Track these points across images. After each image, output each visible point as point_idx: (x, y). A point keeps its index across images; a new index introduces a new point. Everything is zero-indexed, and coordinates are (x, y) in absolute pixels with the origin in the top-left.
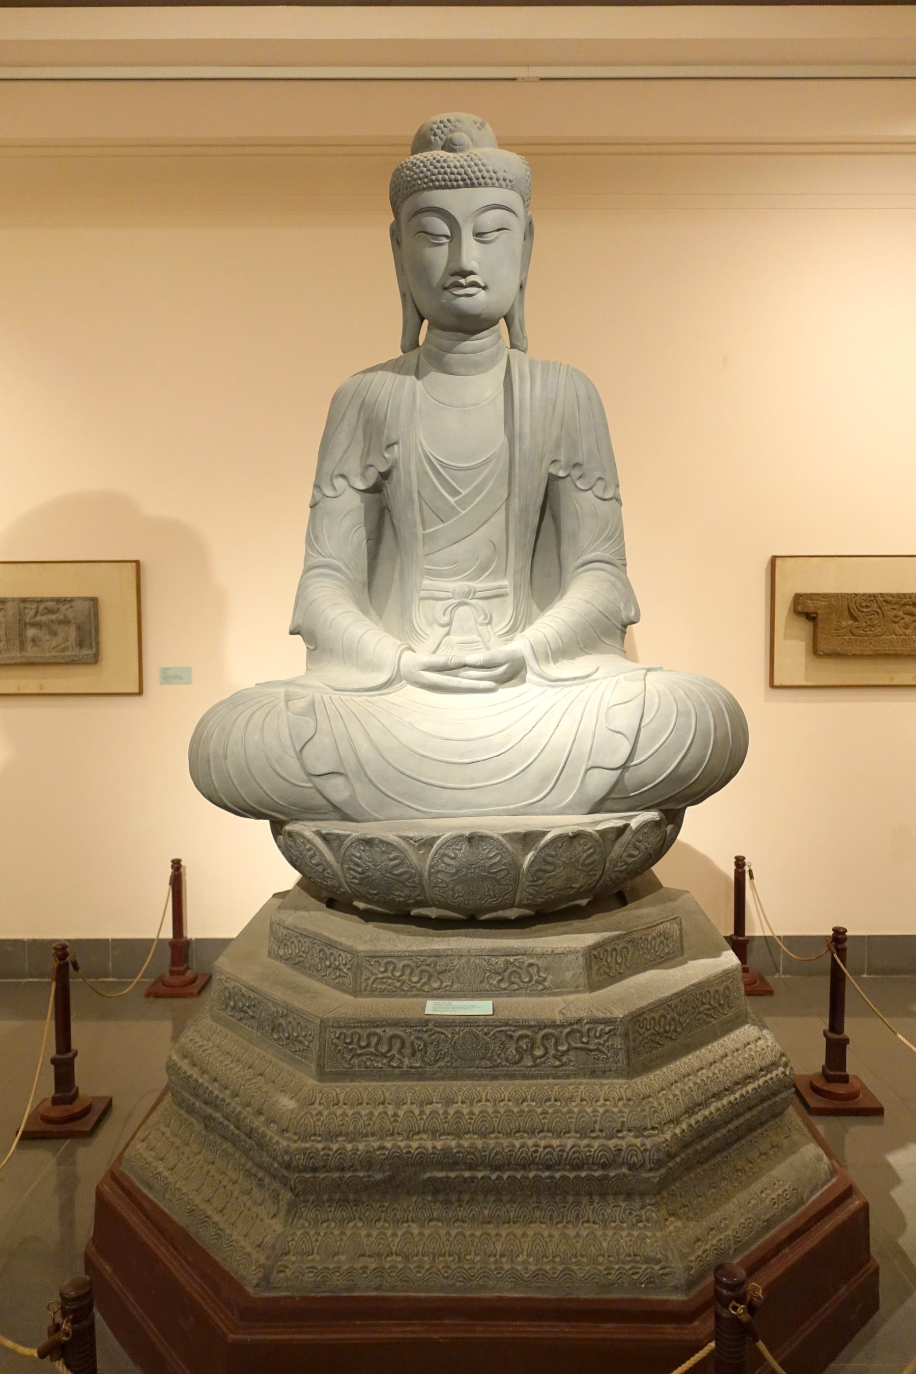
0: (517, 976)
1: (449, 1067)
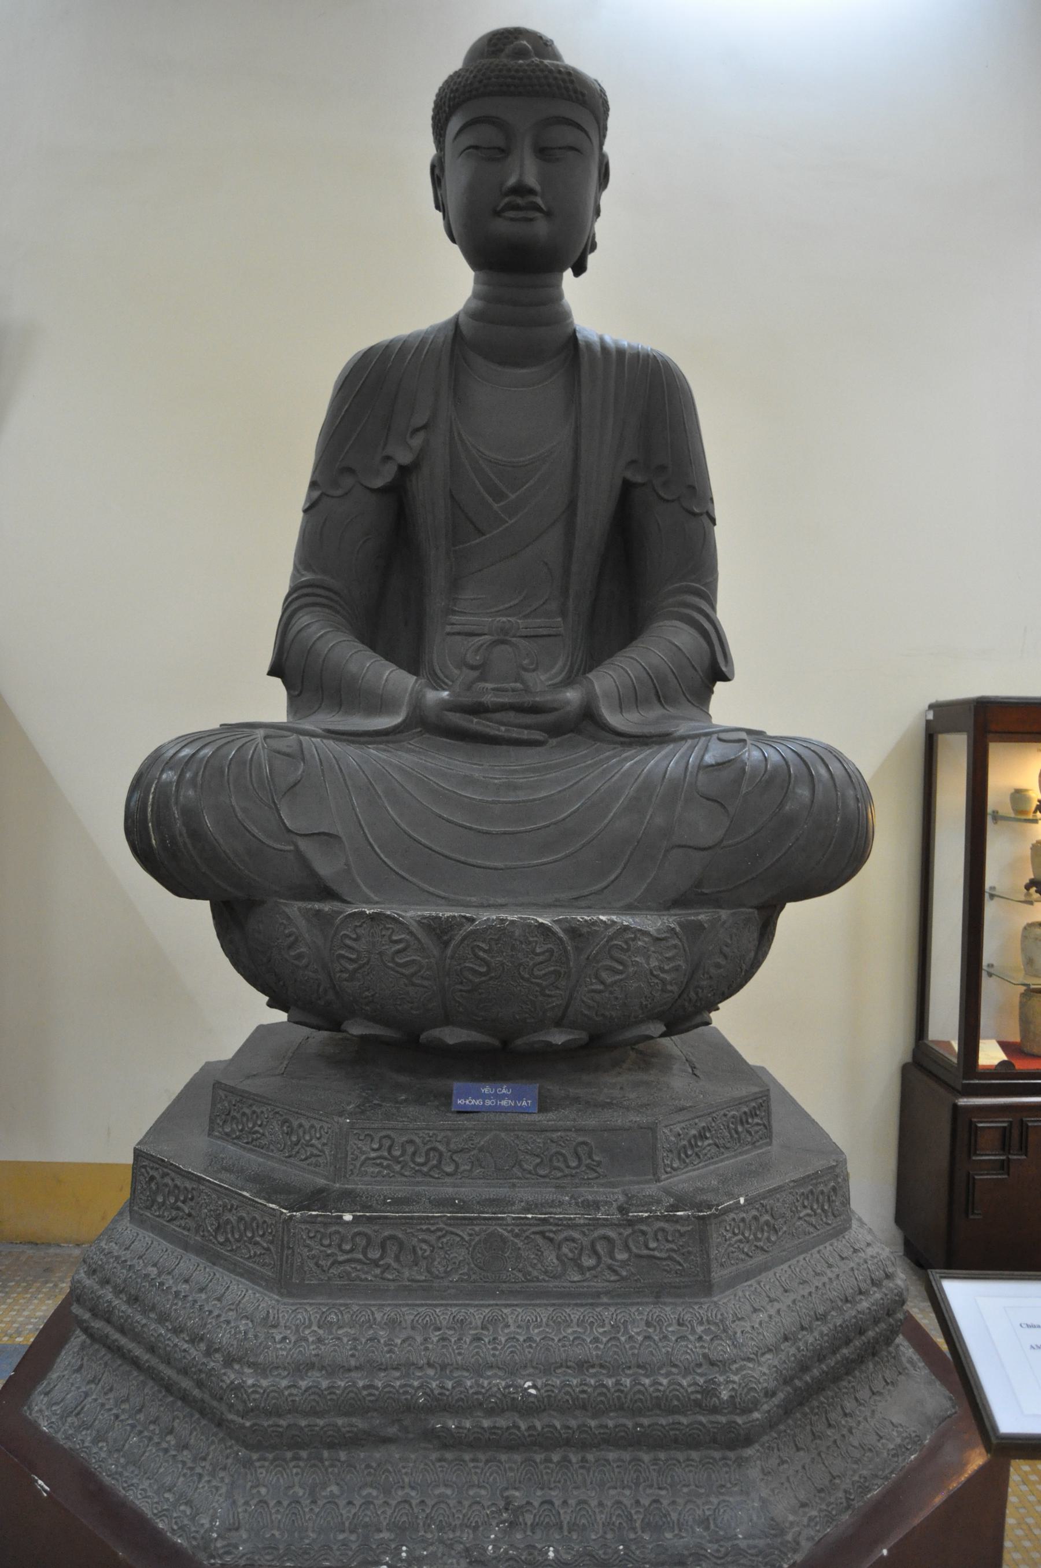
0: (561, 1159)
1: (466, 1281)
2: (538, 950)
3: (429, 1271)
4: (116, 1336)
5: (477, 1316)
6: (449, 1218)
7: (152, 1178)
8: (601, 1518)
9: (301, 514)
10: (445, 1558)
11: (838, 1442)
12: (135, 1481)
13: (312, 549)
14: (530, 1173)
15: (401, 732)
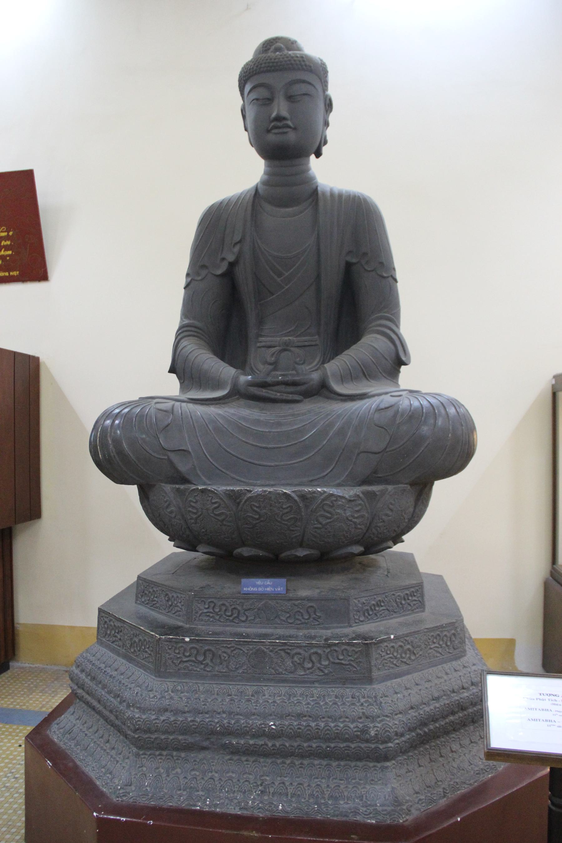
2: (284, 507)
3: (227, 667)
4: (86, 696)
5: (250, 689)
6: (237, 641)
7: (106, 622)
8: (308, 792)
9: (182, 291)
10: (228, 806)
11: (445, 765)
12: (90, 763)
13: (190, 307)
14: (284, 621)
15: (228, 398)
